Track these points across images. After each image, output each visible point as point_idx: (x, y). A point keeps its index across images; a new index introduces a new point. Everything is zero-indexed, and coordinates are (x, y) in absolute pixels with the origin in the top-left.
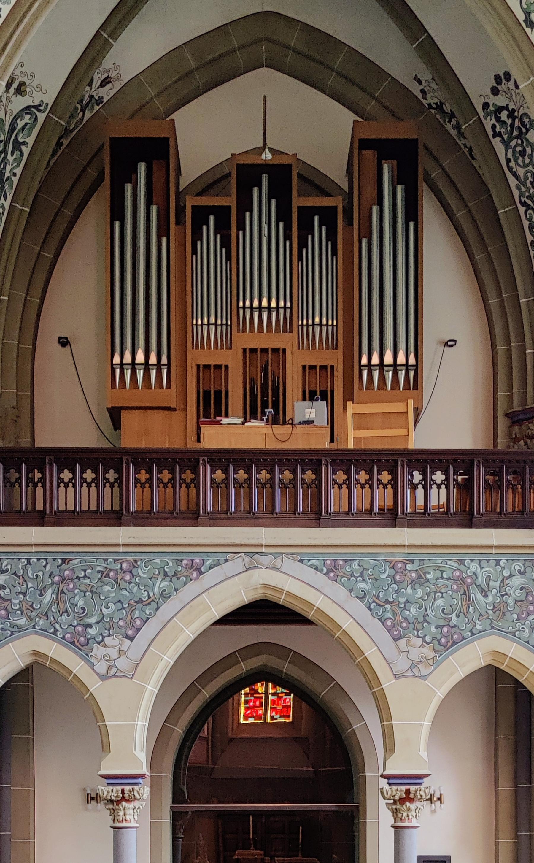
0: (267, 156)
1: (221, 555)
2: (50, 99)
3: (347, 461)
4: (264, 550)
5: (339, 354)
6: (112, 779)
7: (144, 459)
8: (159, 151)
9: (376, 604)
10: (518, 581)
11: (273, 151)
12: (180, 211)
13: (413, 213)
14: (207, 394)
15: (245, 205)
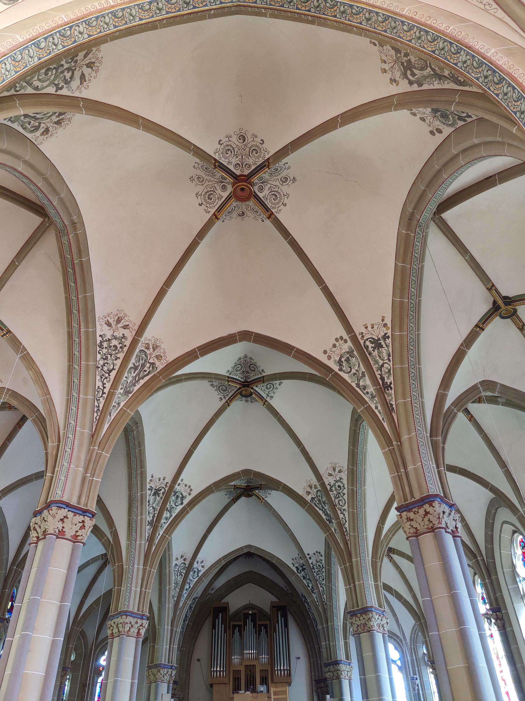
2: (199, 596)
5: (270, 666)
8: (224, 609)
13: (286, 626)
14: (235, 678)
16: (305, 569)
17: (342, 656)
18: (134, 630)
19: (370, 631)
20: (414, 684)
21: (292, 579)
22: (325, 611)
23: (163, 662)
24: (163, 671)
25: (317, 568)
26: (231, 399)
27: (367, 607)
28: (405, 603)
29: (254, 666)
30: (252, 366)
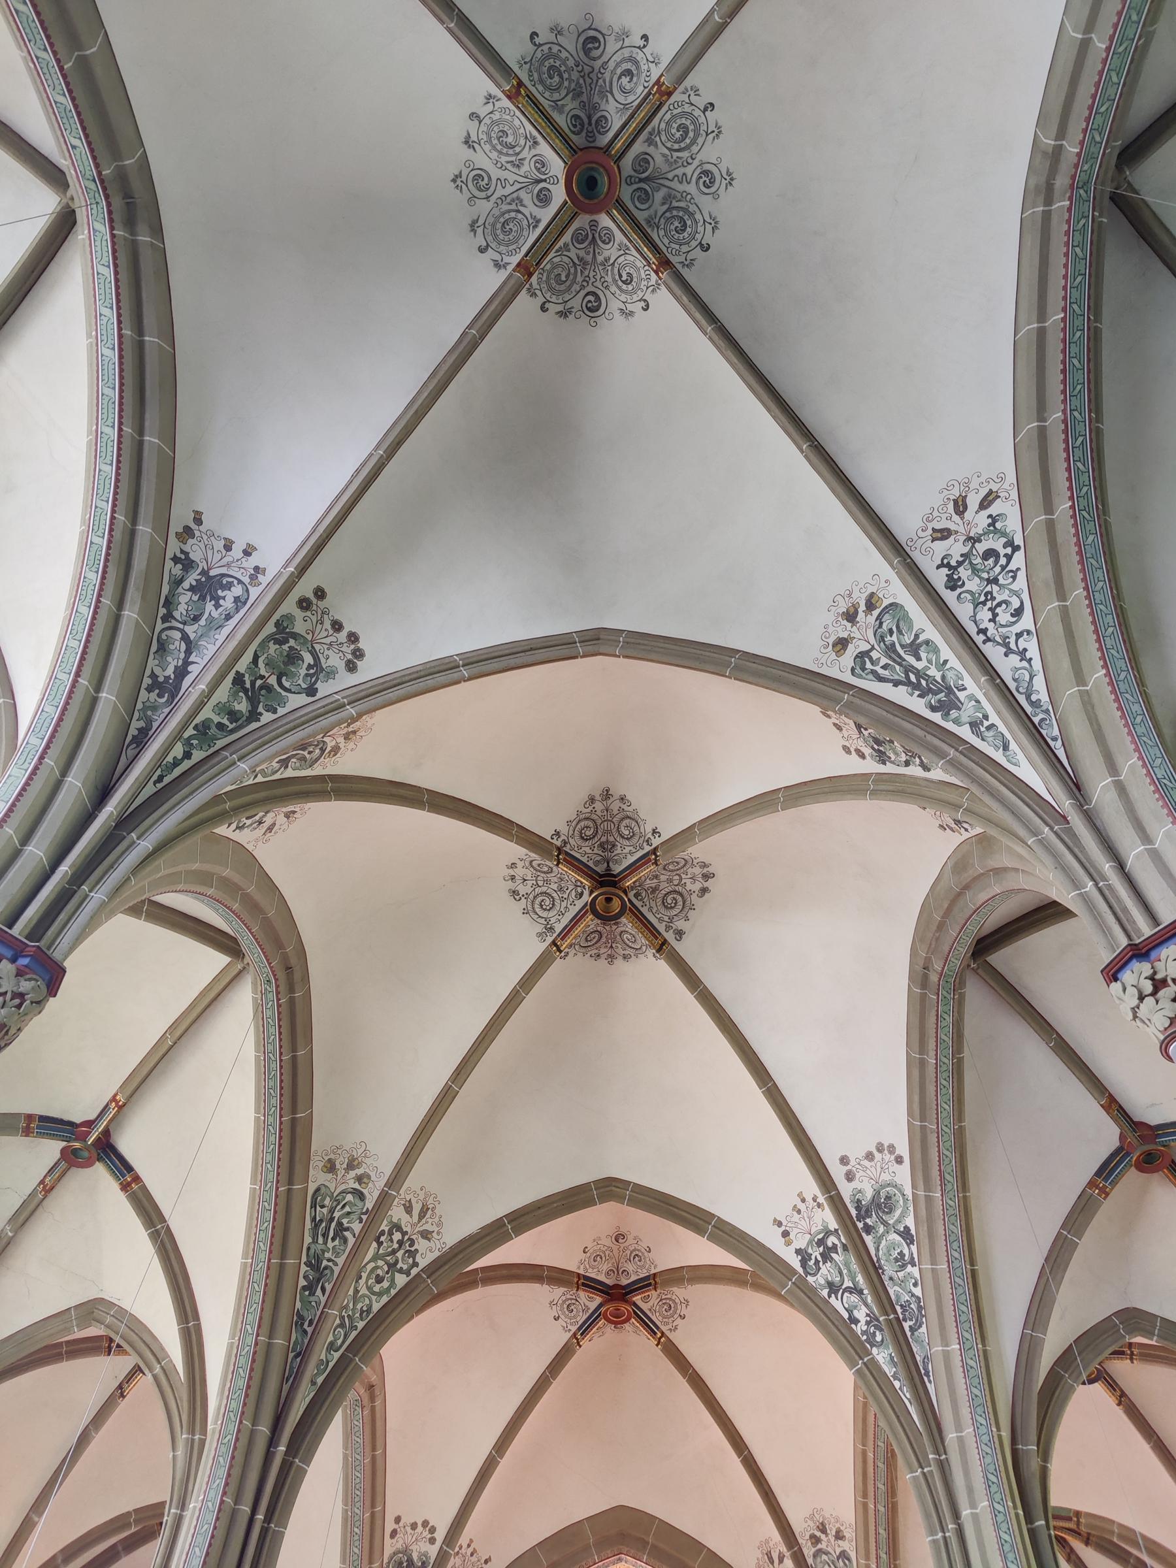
16: (834, 1248)
26: (585, 1328)
30: (627, 821)
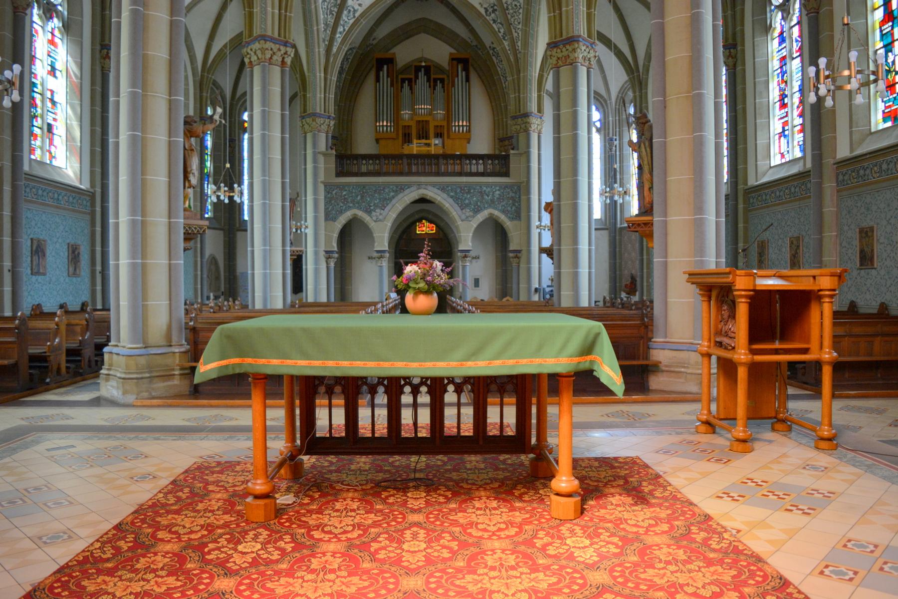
0: (423, 64)
1: (409, 185)
2: (357, 45)
3: (446, 156)
4: (99, 268)
6: (378, 252)
7: (387, 157)
8: (390, 61)
9: (456, 199)
10: (498, 192)
11: (426, 60)
12: (397, 77)
13: (468, 80)
15: (417, 77)
17: (534, 108)
18: (277, 58)
19: (573, 64)
20: (611, 145)
21: (476, 25)
22: (517, 60)
23: (318, 111)
24: (320, 121)
25: (513, 8)
27: (573, 37)
28: (619, 54)
29: (427, 122)
